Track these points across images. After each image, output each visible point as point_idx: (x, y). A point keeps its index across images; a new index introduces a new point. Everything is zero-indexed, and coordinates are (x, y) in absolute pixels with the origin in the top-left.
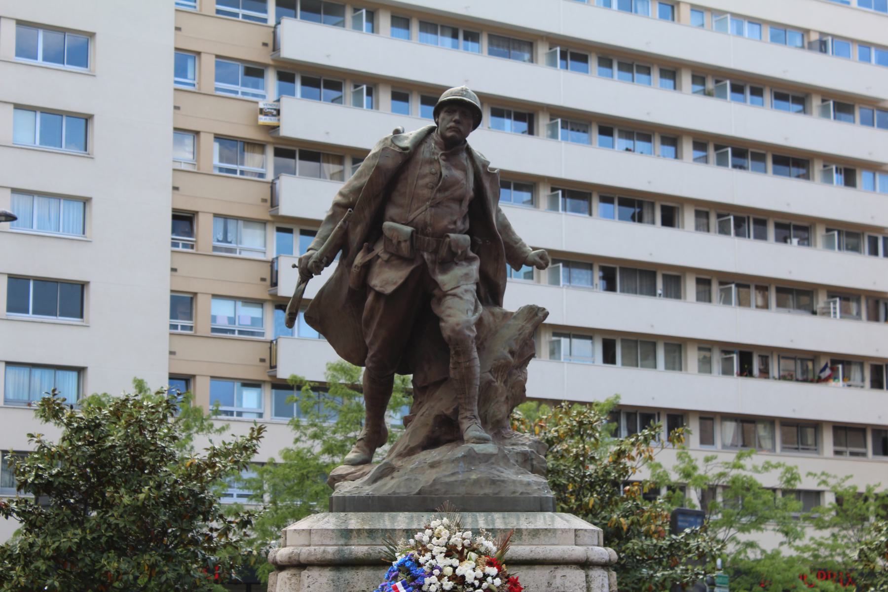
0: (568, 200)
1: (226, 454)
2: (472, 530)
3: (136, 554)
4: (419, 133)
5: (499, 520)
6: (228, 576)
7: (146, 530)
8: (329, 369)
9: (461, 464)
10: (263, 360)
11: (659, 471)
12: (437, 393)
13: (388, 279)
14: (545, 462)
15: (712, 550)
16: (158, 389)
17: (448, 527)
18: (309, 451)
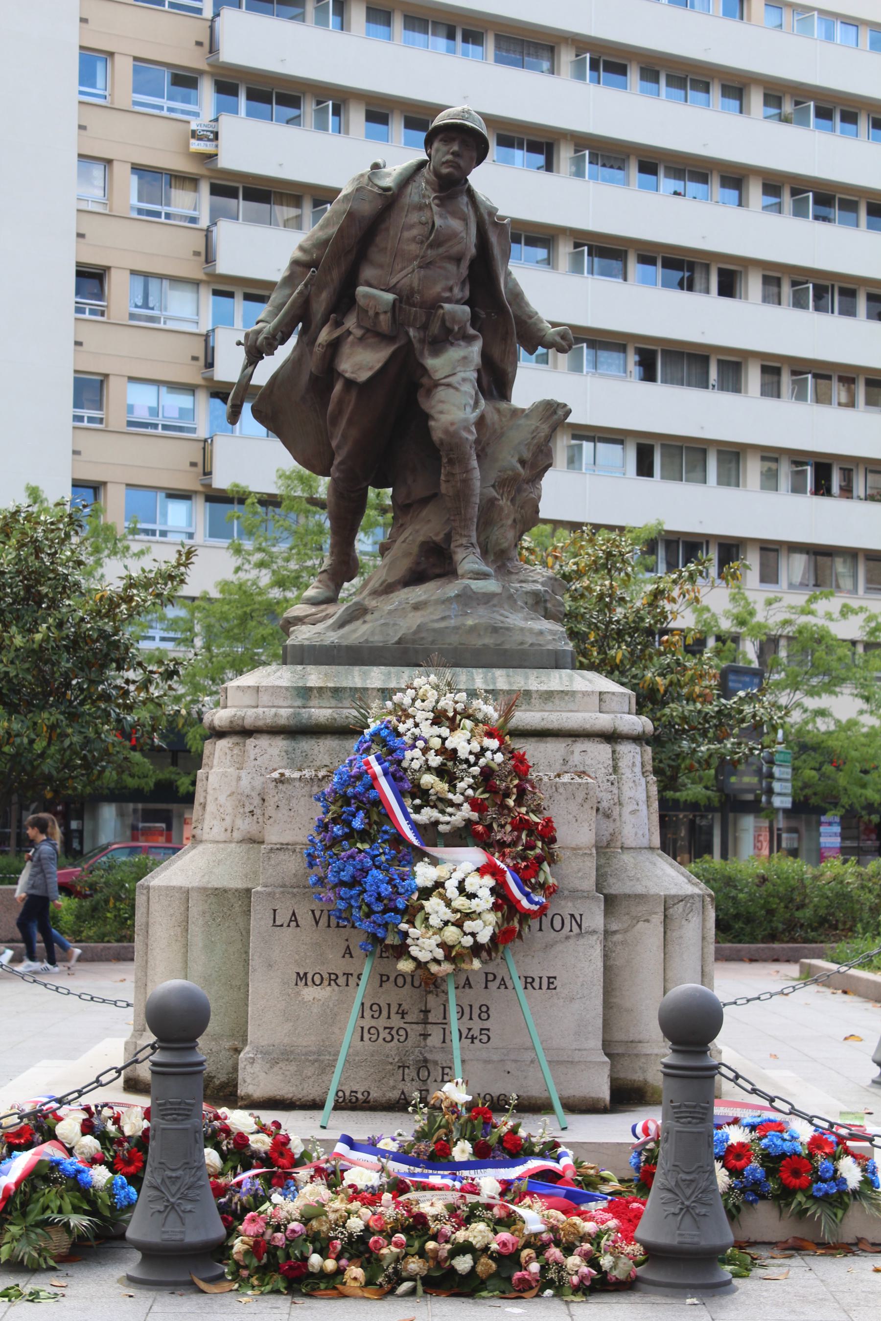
0: (596, 260)
1: (146, 584)
2: (466, 690)
3: (31, 711)
4: (406, 169)
5: (502, 679)
6: (149, 741)
7: (44, 681)
8: (280, 477)
9: (454, 606)
10: (193, 464)
11: (706, 616)
12: (424, 513)
13: (361, 362)
14: (563, 605)
15: (772, 718)
16: (57, 499)
17: (436, 687)
18: (254, 583)
